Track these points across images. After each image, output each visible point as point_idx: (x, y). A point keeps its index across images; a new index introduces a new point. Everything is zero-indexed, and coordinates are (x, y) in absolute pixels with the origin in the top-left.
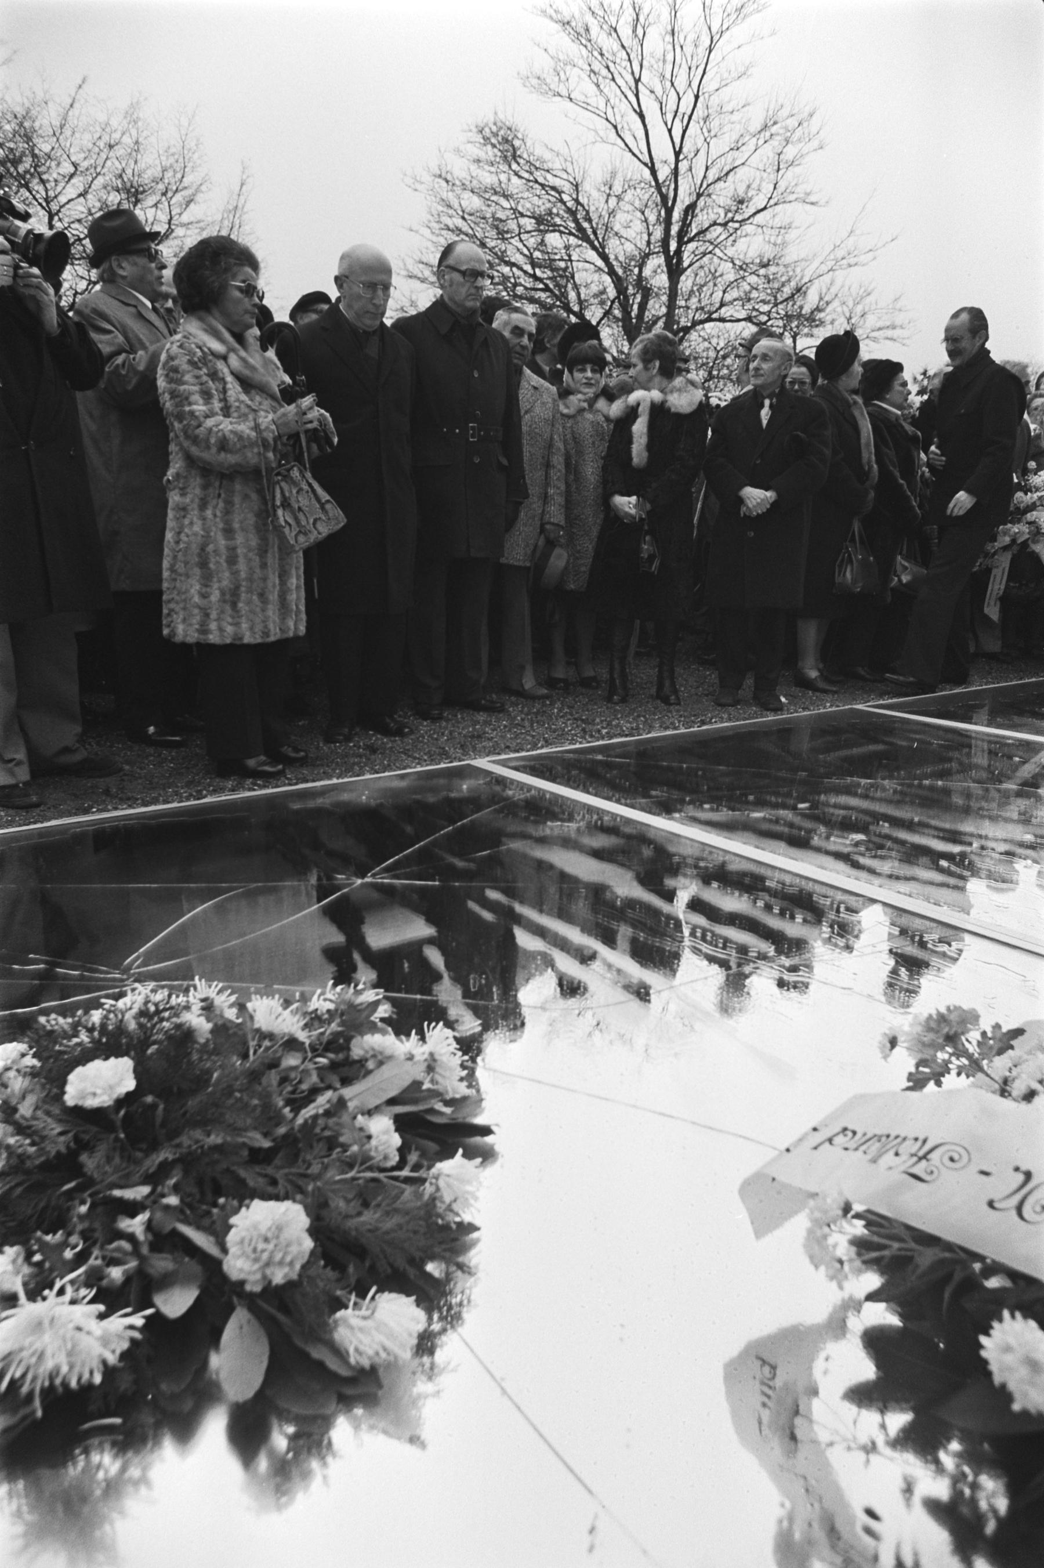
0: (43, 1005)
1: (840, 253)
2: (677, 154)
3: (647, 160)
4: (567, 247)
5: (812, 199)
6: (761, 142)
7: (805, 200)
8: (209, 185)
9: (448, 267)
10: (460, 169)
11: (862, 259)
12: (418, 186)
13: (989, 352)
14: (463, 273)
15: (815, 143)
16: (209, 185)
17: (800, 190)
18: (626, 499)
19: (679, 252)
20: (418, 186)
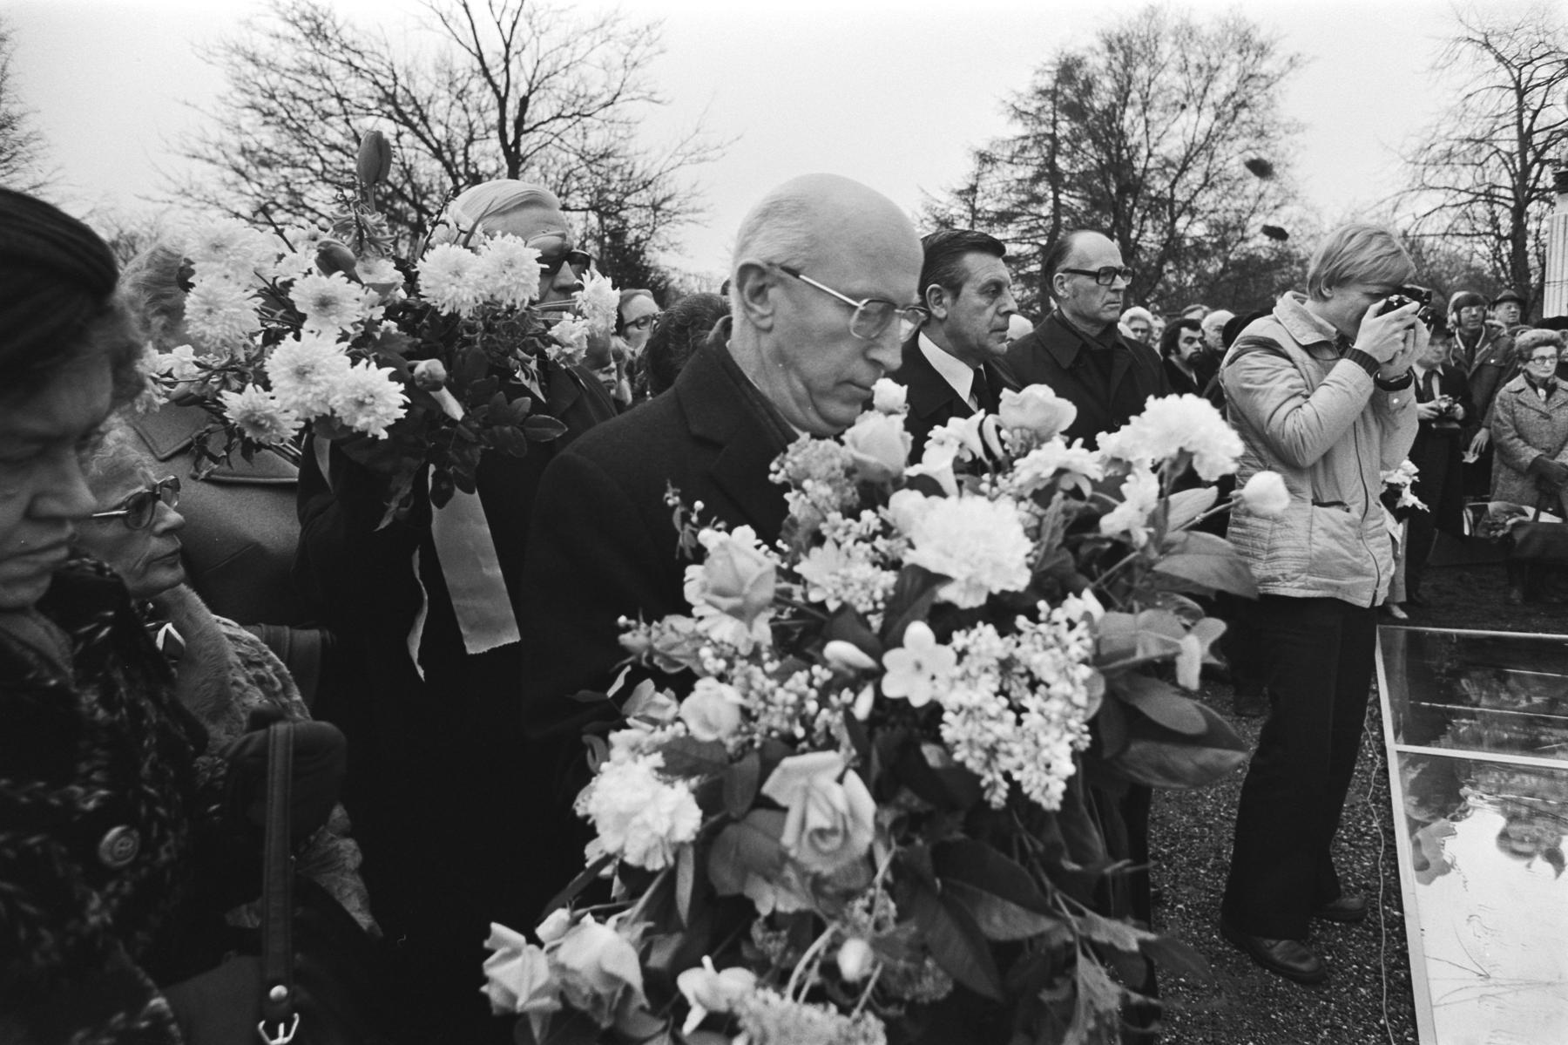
0: (415, 654)
1: (688, 149)
2: (508, 46)
3: (474, 50)
4: (399, 135)
5: (656, 97)
6: (598, 41)
7: (650, 98)
8: (644, 197)
9: (1067, 271)
10: (265, 47)
11: (709, 154)
12: (213, 59)
13: (1181, 395)
14: (1095, 275)
15: (655, 48)
16: (644, 197)
17: (646, 89)
18: (235, 629)
19: (517, 143)
20: (213, 59)
